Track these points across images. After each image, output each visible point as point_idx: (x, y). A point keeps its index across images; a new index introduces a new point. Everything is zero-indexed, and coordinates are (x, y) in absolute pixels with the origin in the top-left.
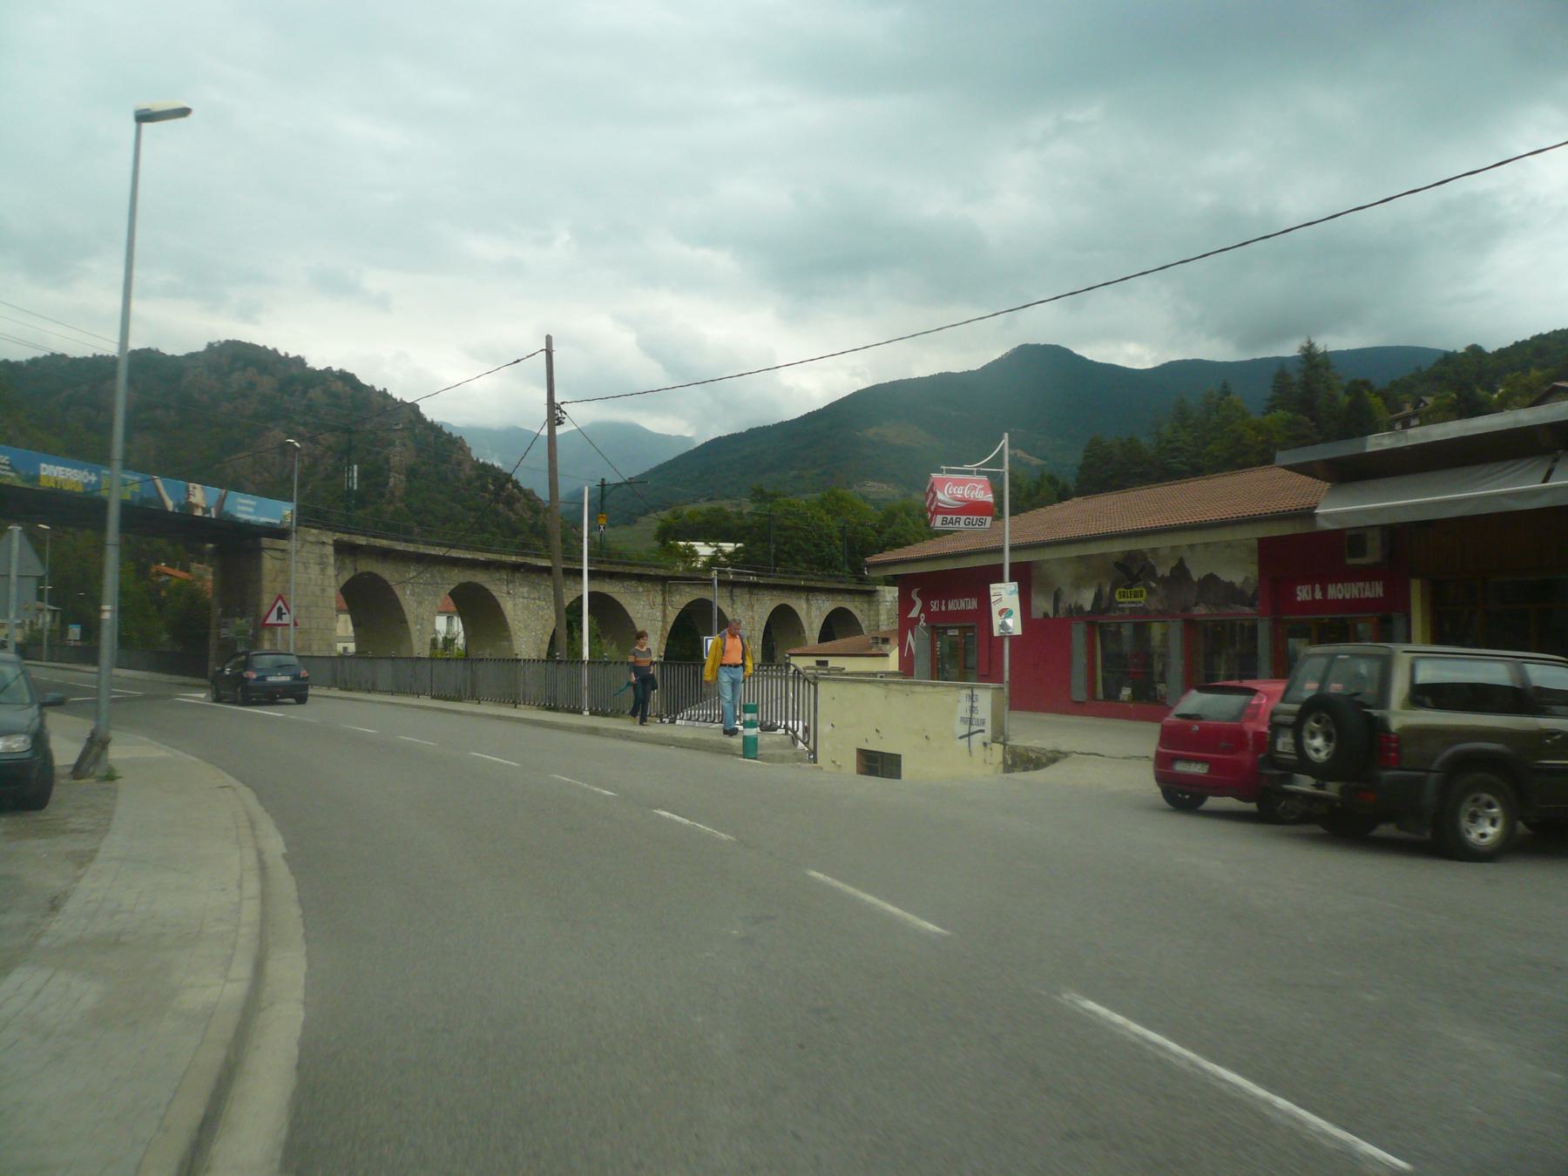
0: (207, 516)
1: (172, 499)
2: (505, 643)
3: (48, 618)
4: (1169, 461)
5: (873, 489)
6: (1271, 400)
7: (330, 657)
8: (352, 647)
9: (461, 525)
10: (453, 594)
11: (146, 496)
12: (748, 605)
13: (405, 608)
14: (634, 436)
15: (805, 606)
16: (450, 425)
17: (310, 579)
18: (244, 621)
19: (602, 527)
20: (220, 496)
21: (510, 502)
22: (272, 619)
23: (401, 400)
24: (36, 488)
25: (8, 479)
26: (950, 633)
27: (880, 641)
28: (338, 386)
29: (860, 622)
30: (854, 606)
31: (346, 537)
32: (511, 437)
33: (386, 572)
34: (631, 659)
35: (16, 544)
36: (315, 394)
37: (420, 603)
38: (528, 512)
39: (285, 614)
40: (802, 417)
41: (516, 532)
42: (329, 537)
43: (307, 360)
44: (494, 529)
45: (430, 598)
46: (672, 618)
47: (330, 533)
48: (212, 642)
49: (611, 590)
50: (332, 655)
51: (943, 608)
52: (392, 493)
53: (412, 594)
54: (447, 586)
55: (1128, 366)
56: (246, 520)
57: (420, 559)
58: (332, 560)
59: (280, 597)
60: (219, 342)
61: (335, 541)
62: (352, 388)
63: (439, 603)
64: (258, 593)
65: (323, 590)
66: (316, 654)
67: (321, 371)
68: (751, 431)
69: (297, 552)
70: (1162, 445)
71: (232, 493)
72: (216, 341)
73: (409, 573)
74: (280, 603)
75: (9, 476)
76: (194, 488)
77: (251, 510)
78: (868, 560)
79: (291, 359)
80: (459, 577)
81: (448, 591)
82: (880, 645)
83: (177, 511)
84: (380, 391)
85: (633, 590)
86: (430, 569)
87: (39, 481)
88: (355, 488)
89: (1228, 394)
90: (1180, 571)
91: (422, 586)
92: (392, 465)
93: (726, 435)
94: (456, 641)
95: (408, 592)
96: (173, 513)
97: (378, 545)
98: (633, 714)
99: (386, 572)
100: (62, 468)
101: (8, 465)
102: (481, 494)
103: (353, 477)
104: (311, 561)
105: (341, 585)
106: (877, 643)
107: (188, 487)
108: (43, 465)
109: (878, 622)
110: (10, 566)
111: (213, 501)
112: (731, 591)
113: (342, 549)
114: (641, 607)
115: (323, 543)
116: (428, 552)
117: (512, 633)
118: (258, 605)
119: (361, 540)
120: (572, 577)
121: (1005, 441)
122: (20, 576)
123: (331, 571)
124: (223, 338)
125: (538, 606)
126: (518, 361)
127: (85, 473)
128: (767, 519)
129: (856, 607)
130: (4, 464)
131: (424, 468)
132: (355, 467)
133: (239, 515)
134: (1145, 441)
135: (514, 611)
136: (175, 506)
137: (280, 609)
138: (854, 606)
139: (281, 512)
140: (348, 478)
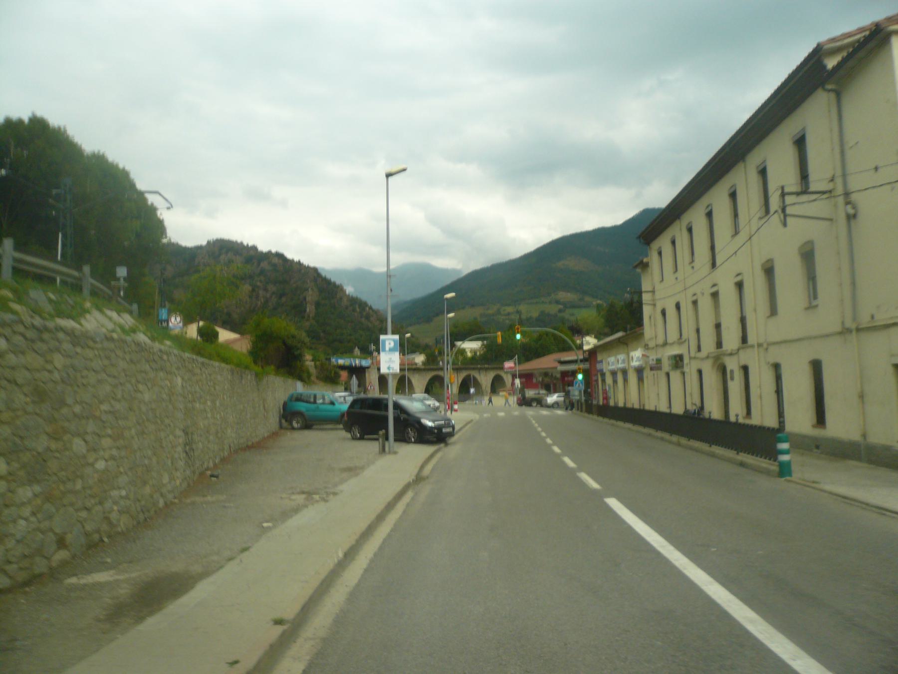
14: (425, 271)
16: (323, 269)
28: (275, 260)
32: (361, 275)
36: (264, 265)
46: (460, 381)
52: (309, 316)
60: (213, 239)
84: (297, 262)
90: (552, 375)
118: (366, 385)
121: (517, 356)
124: (215, 239)
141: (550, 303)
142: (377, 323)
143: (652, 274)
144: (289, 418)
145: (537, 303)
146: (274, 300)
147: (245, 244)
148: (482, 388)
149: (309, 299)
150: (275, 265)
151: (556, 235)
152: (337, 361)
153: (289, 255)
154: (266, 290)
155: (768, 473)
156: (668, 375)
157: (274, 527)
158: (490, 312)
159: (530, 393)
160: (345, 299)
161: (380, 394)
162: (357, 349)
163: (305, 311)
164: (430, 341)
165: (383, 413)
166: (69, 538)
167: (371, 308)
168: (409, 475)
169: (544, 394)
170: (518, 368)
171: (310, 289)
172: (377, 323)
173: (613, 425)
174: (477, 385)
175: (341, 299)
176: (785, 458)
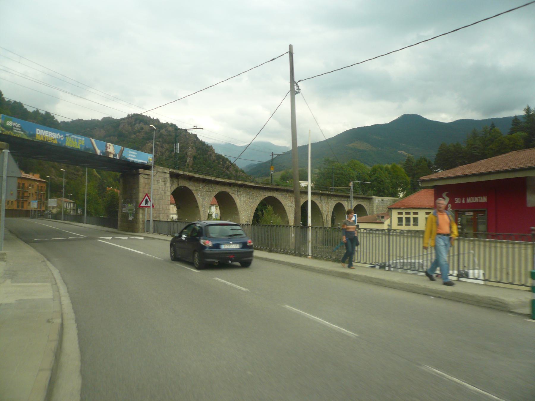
0: (115, 158)
1: (99, 149)
2: (236, 216)
3: (72, 205)
4: (472, 152)
6: (511, 129)
7: (168, 221)
8: (176, 217)
10: (217, 197)
11: (87, 147)
12: (327, 203)
13: (198, 201)
15: (347, 203)
17: (160, 188)
18: (132, 205)
19: (272, 171)
20: (121, 149)
22: (143, 204)
23: (191, 133)
24: (34, 140)
25: (20, 135)
26: (467, 214)
27: (380, 217)
28: (170, 129)
29: (366, 210)
30: (364, 204)
31: (175, 171)
33: (191, 186)
34: (344, 227)
35: (6, 159)
36: (163, 131)
37: (204, 199)
38: (234, 171)
39: (149, 202)
42: (168, 171)
43: (160, 120)
45: (208, 197)
47: (169, 169)
48: (120, 214)
49: (277, 196)
50: (168, 220)
51: (463, 202)
52: (188, 165)
53: (201, 196)
54: (214, 193)
55: (442, 122)
56: (132, 161)
57: (204, 181)
58: (169, 179)
59: (147, 195)
60: (131, 114)
61: (170, 172)
63: (211, 200)
64: (137, 193)
65: (165, 193)
66: (162, 220)
67: (165, 124)
69: (154, 176)
70: (469, 146)
71: (126, 149)
72: (130, 114)
73: (200, 187)
74: (147, 197)
75: (20, 133)
76: (110, 145)
77: (135, 156)
78: (421, 178)
79: (155, 120)
80: (219, 189)
81: (215, 195)
82: (380, 219)
83: (101, 155)
85: (285, 196)
86: (208, 185)
87: (36, 137)
88: (178, 153)
89: (494, 127)
91: (204, 192)
92: (188, 155)
93: (300, 146)
94: (212, 215)
95: (199, 195)
96: (100, 155)
97: (187, 174)
98: (343, 261)
99: (191, 186)
100: (47, 132)
101: (20, 128)
102: (218, 165)
103: (177, 148)
104: (160, 180)
105: (173, 191)
106: (379, 218)
107: (106, 146)
108: (38, 130)
109: (373, 210)
110: (3, 172)
111: (118, 151)
112: (321, 197)
113: (173, 176)
114: (288, 203)
115: (165, 173)
116: (207, 178)
117: (239, 212)
118: (137, 198)
119: (181, 172)
120: (262, 190)
122: (7, 177)
123: (168, 184)
125: (249, 202)
126: (273, 59)
127: (58, 135)
128: (332, 170)
129: (365, 204)
130: (18, 128)
131: (199, 156)
132: (178, 144)
133: (129, 158)
134: (464, 146)
135: (240, 203)
136: (101, 152)
137: (146, 200)
138: (364, 204)
139: (146, 158)
140: (175, 148)
142: (234, 172)
146: (167, 153)
147: (169, 123)
148: (322, 217)
149: (189, 153)
154: (162, 147)
160: (213, 155)
161: (146, 205)
163: (186, 162)
165: (63, 218)
172: (234, 172)
175: (211, 155)
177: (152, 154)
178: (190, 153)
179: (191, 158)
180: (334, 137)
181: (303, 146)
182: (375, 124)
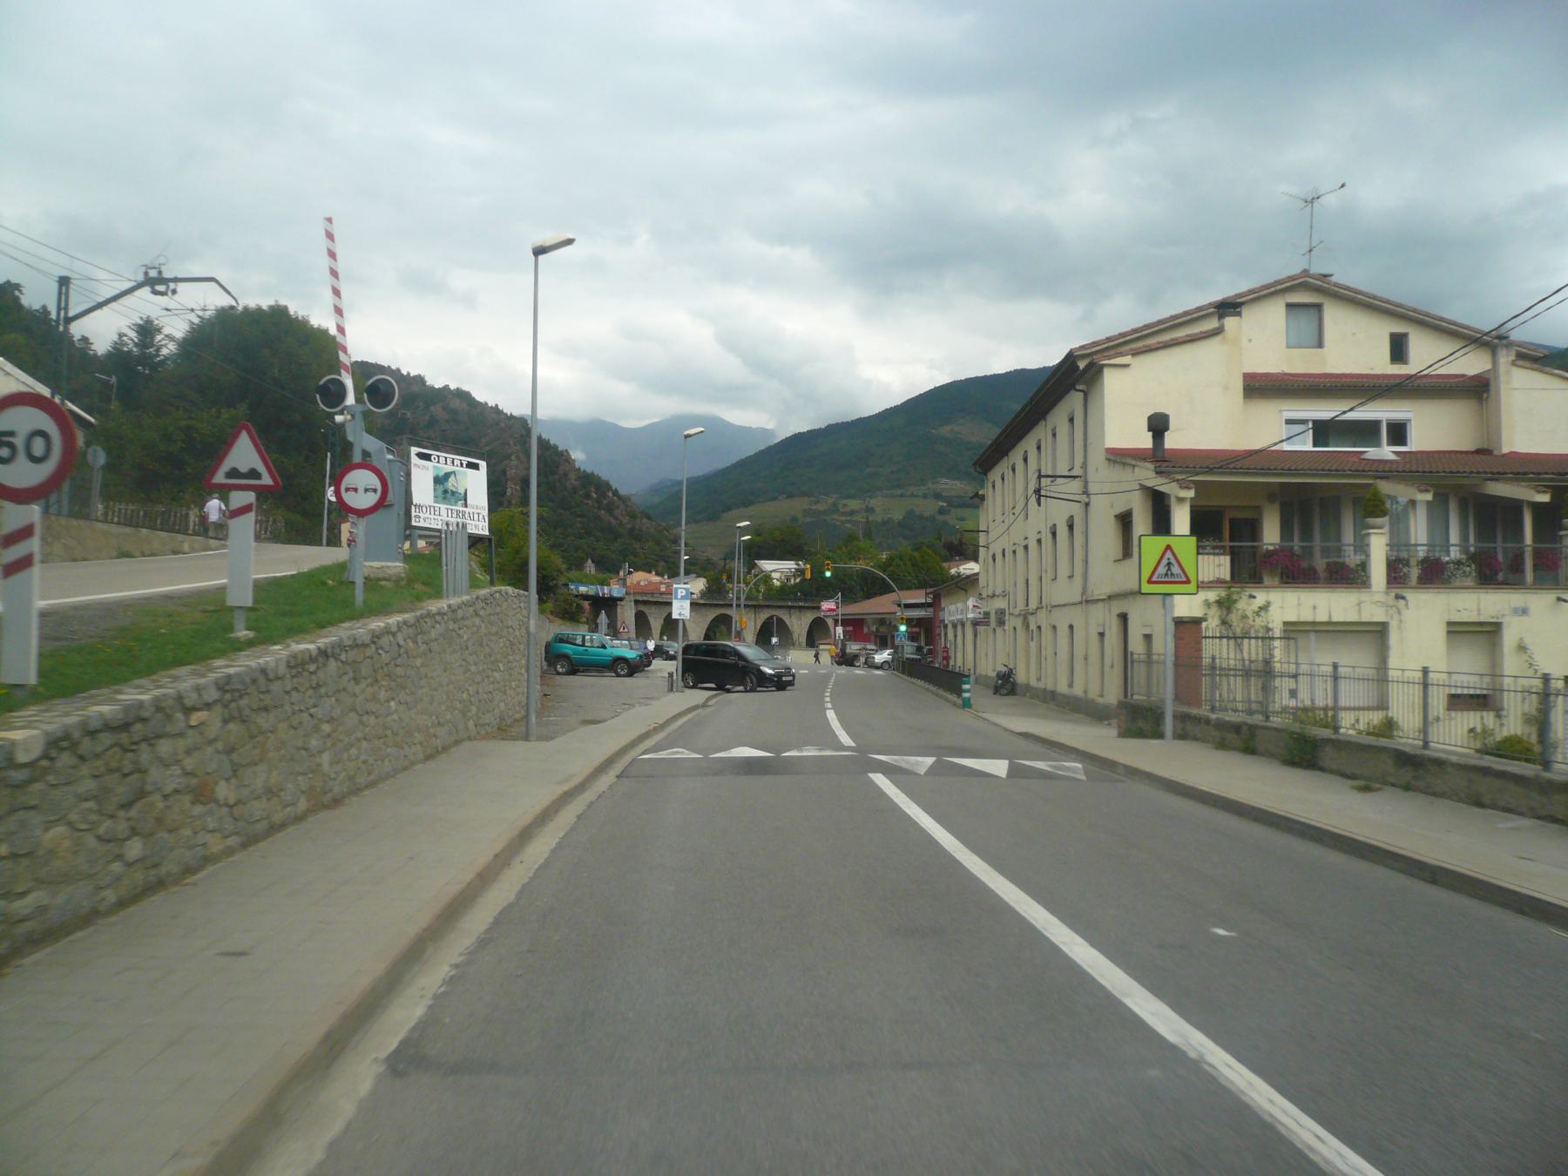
5: (947, 487)
9: (570, 530)
14: (715, 427)
21: (610, 508)
23: (511, 414)
28: (456, 404)
36: (437, 410)
38: (627, 518)
40: (879, 413)
41: (617, 536)
43: (426, 379)
44: (598, 534)
62: (468, 405)
68: (830, 426)
90: (890, 623)
92: (508, 476)
118: (616, 625)
141: (925, 496)
142: (626, 520)
143: (987, 510)
144: (552, 661)
145: (901, 496)
148: (792, 639)
150: (454, 412)
151: (942, 379)
152: (577, 589)
153: (480, 396)
155: (955, 704)
156: (994, 630)
157: (630, 709)
158: (820, 507)
159: (853, 648)
160: (572, 476)
162: (590, 561)
164: (714, 554)
166: (434, 739)
167: (616, 493)
168: (701, 701)
169: (873, 650)
170: (840, 611)
171: (513, 457)
173: (913, 683)
174: (784, 631)
175: (566, 475)
176: (966, 695)
177: (705, 639)
178: (513, 471)
179: (515, 484)
180: (902, 404)
181: (811, 431)
182: (1015, 368)
